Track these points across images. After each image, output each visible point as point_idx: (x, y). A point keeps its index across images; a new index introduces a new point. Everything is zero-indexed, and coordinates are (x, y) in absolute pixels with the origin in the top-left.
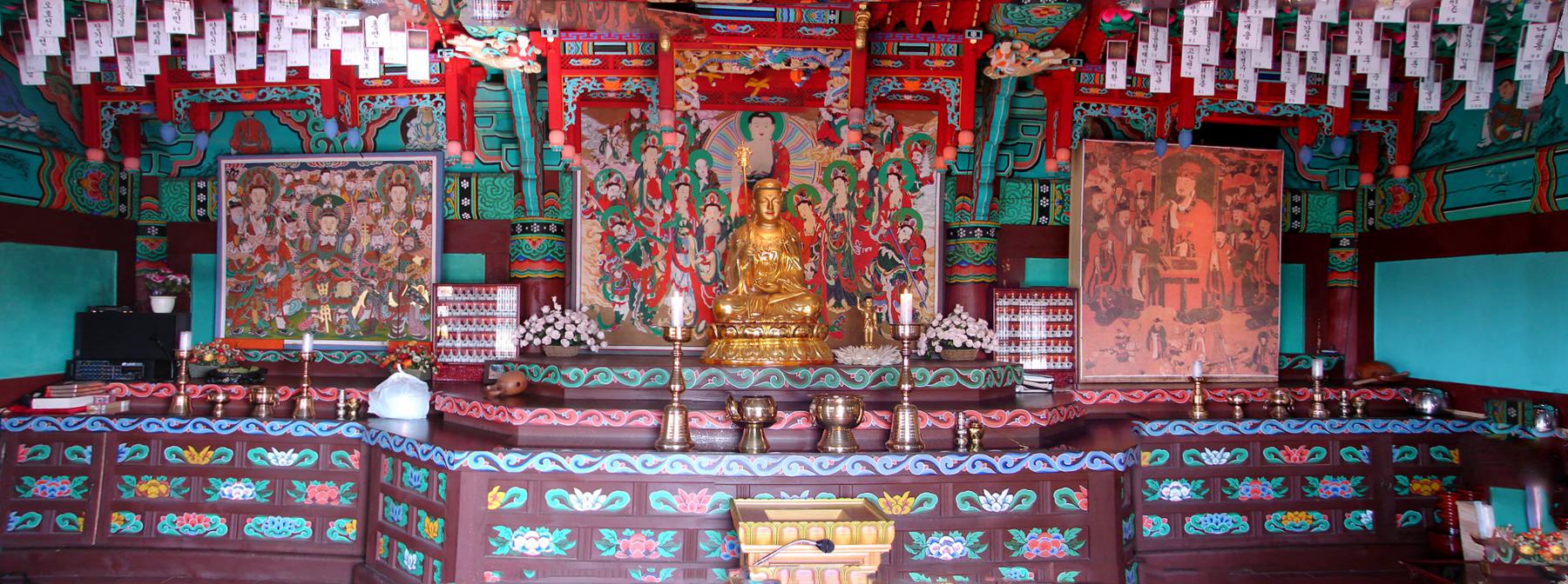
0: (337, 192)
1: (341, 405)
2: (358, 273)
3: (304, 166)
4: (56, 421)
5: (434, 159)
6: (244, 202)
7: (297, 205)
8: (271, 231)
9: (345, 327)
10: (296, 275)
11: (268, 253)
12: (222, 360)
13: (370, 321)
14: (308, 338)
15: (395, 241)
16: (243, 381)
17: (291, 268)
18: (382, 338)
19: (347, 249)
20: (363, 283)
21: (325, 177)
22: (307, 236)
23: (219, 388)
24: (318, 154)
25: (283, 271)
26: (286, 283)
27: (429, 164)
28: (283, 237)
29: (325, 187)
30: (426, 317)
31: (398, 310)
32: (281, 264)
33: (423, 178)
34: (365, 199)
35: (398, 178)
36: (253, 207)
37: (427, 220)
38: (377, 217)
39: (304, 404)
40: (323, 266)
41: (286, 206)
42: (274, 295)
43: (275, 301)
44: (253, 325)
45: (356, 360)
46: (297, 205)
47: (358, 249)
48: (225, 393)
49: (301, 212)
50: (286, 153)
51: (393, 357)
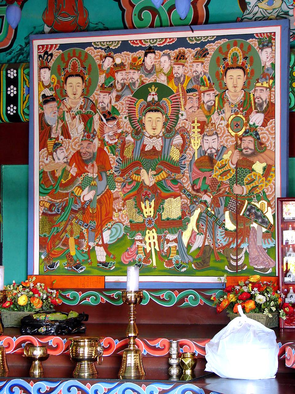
0: (162, 79)
1: (174, 361)
2: (188, 186)
3: (125, 46)
4: (165, 185)
5: (277, 30)
6: (56, 97)
7: (118, 98)
8: (89, 134)
9: (174, 257)
10: (118, 191)
11: (86, 163)
12: (37, 304)
13: (204, 251)
14: (133, 271)
15: (230, 143)
16: (63, 329)
17: (111, 183)
18: (218, 272)
19: (175, 155)
20: (194, 200)
21: (150, 60)
22: (129, 138)
23: (35, 340)
24: (141, 29)
25: (102, 186)
26: (105, 200)
27: (271, 37)
28: (102, 141)
29: (149, 72)
30: (270, 244)
31: (236, 234)
32: (100, 178)
33: (265, 56)
34: (196, 87)
35: (235, 58)
36: (68, 102)
37: (269, 114)
38: (210, 110)
39: (131, 360)
40: (147, 178)
41: (105, 100)
42: (92, 216)
43: (93, 224)
44: (69, 257)
45: (190, 302)
46: (118, 98)
47: (189, 153)
48: (43, 346)
49: (122, 106)
50: (105, 29)
51: (232, 298)
